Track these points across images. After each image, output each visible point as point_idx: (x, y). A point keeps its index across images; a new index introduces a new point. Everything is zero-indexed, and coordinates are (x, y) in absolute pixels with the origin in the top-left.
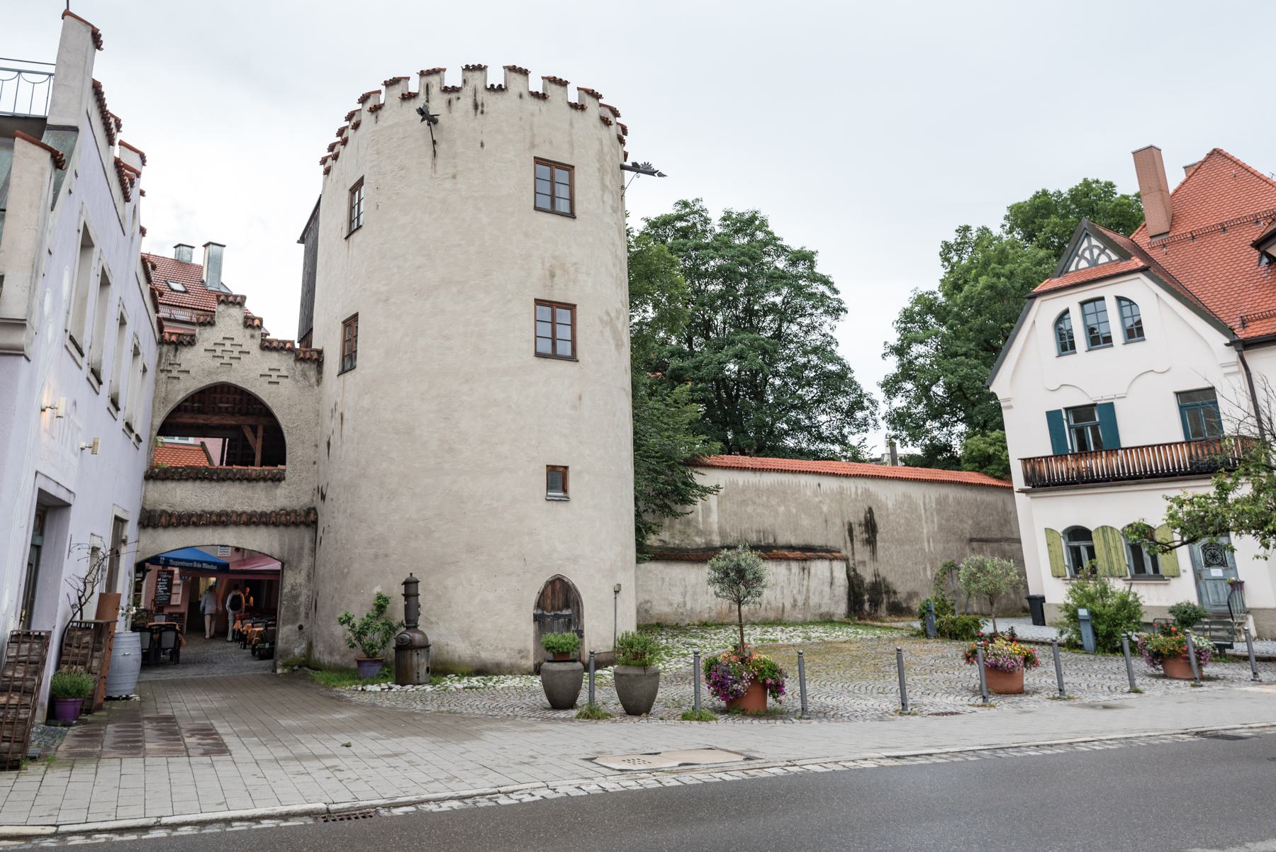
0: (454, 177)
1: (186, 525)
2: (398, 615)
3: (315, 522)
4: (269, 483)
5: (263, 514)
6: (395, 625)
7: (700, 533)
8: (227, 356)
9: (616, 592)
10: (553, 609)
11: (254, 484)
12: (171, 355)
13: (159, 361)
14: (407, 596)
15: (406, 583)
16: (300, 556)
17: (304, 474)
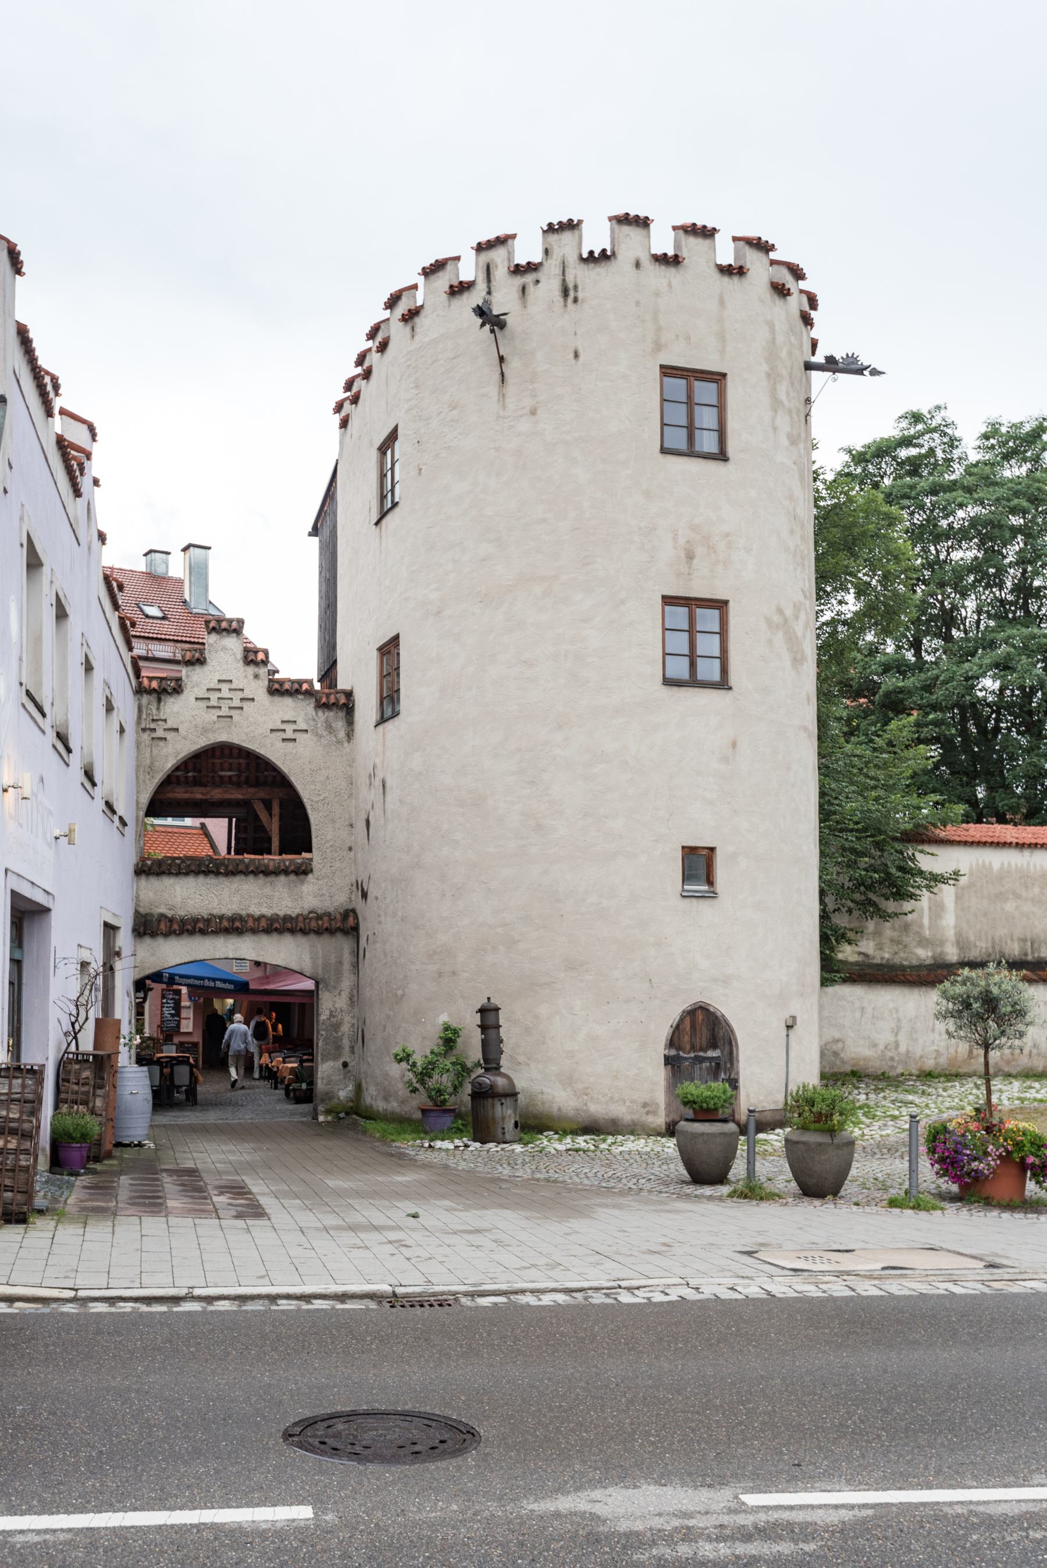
0: (533, 412)
1: (191, 933)
4: (292, 877)
5: (287, 918)
6: (469, 1065)
7: (923, 942)
9: (789, 1027)
10: (693, 1048)
11: (272, 878)
13: (139, 717)
14: (484, 1027)
15: (482, 1011)
17: (337, 865)
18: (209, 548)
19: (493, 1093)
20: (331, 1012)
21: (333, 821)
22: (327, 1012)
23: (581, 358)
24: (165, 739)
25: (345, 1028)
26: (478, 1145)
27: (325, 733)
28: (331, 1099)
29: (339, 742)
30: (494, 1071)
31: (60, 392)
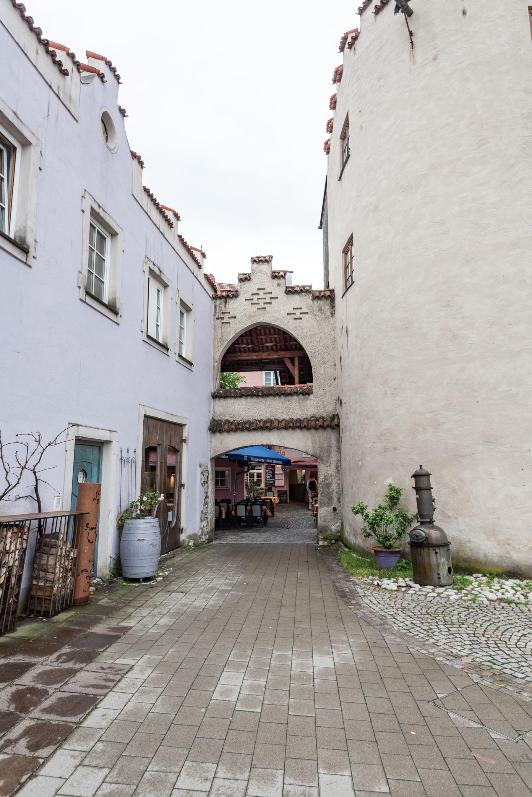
0: (435, 59)
1: (242, 430)
2: (412, 509)
3: (338, 426)
4: (301, 397)
5: (299, 421)
6: (410, 517)
8: (261, 302)
11: (289, 398)
12: (223, 306)
13: (215, 312)
14: (418, 489)
15: (416, 476)
16: (329, 453)
17: (327, 388)
18: (292, 272)
19: (428, 543)
20: (325, 476)
21: (324, 363)
22: (323, 477)
23: (468, 13)
24: (229, 323)
25: (334, 487)
26: (417, 586)
27: (318, 313)
28: (326, 531)
29: (327, 318)
30: (428, 525)
31: (120, 81)
